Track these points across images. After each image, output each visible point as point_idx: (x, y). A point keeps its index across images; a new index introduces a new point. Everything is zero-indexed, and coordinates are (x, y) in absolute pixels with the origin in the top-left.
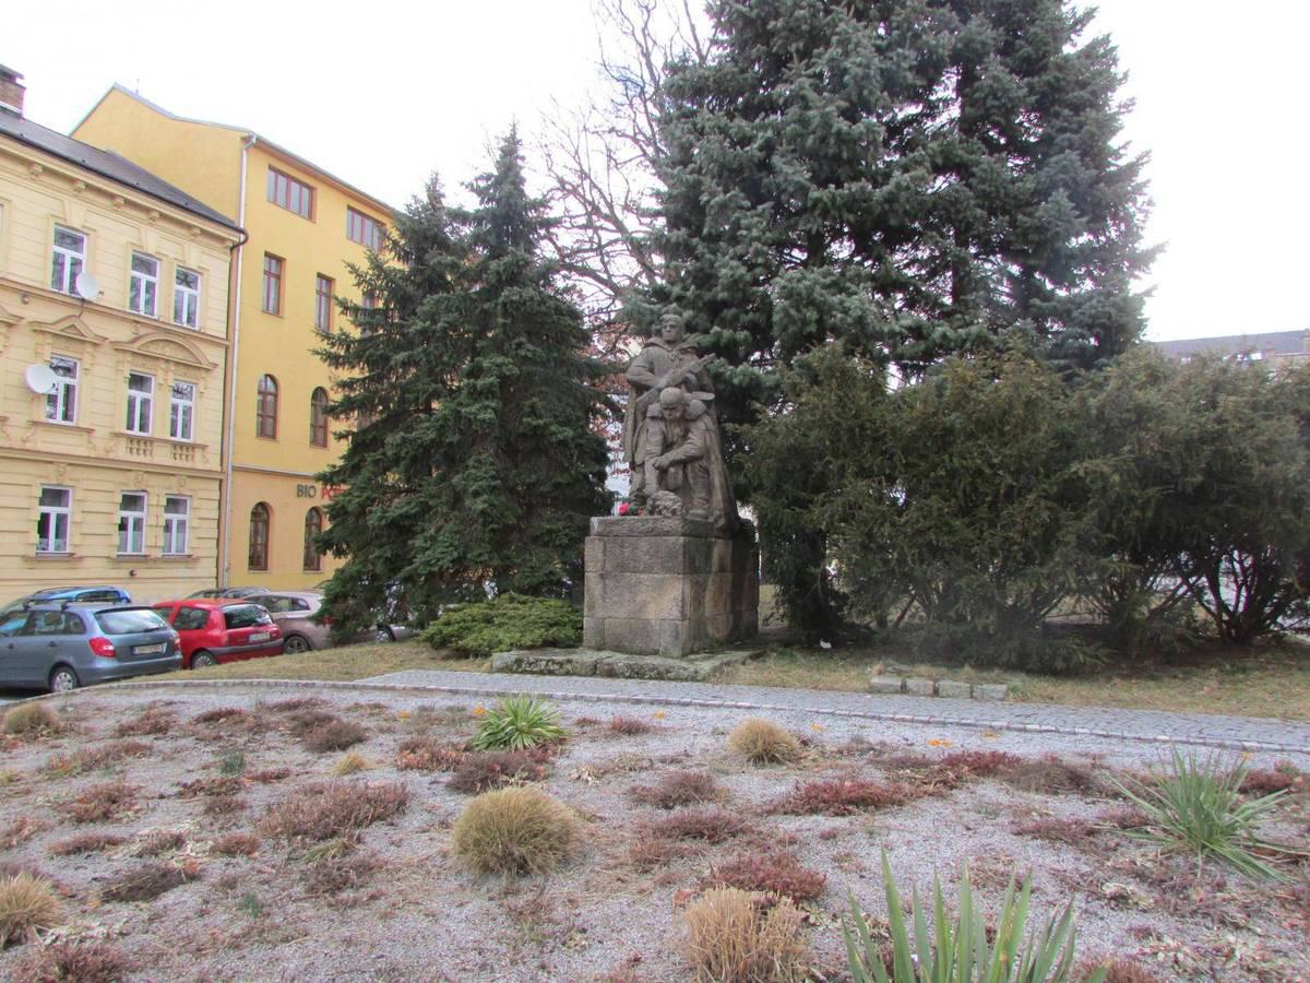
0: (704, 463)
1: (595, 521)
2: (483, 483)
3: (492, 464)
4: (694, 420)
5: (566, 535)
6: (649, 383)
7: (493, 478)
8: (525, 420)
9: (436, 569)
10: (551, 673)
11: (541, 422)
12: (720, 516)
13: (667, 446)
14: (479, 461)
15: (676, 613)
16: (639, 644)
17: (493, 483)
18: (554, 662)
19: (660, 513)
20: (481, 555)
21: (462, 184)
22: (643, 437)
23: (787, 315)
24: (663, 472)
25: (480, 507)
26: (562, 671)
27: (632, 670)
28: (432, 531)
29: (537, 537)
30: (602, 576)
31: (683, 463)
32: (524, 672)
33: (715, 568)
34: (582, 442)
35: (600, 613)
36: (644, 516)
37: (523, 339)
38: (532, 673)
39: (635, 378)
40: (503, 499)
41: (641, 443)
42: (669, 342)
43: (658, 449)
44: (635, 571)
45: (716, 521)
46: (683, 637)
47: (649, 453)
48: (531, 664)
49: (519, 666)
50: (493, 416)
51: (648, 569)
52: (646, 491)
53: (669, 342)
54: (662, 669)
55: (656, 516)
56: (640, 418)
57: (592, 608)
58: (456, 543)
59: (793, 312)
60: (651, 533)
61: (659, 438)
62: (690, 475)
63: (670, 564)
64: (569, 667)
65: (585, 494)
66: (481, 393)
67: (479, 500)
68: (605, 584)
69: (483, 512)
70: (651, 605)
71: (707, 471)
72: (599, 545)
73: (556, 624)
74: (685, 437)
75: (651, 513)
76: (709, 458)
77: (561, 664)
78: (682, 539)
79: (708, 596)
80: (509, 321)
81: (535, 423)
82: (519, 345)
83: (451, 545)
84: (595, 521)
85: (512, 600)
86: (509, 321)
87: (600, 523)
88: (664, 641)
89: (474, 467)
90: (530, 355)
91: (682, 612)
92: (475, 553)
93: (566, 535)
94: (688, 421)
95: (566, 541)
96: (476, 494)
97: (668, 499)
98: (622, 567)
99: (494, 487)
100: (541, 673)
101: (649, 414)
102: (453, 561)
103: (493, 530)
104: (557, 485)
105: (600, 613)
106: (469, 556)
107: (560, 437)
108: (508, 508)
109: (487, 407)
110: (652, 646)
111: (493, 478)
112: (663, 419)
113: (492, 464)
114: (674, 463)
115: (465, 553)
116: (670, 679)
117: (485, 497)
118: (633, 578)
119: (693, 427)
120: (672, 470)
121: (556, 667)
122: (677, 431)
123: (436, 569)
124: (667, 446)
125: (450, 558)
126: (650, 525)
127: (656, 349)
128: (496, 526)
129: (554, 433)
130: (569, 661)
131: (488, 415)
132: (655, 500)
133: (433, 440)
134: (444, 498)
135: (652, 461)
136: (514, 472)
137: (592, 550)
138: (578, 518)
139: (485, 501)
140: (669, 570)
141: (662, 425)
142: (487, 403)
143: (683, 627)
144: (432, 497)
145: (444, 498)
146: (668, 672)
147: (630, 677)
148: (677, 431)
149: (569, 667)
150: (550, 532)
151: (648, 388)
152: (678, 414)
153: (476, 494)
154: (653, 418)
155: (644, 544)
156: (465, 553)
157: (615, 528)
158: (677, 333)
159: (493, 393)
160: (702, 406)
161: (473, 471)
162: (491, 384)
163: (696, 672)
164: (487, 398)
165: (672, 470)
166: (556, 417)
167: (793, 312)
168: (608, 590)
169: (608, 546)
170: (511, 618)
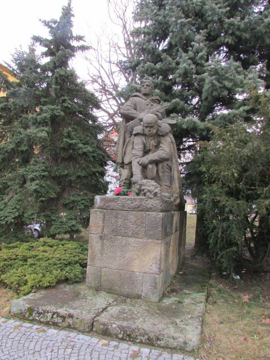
0: (169, 163)
1: (98, 198)
2: (37, 174)
3: (43, 163)
4: (163, 136)
5: (82, 204)
6: (134, 115)
7: (44, 171)
8: (64, 139)
9: (4, 223)
10: (55, 325)
11: (74, 141)
12: (177, 197)
13: (146, 152)
14: (36, 162)
15: (155, 269)
16: (126, 290)
17: (43, 174)
18: (58, 315)
19: (145, 194)
20: (32, 214)
21: (40, 20)
22: (129, 147)
23: (213, 85)
24: (144, 167)
25: (34, 188)
26: (65, 324)
27: (125, 332)
28: (6, 200)
29: (66, 204)
30: (101, 237)
31: (156, 163)
32: (33, 321)
33: (174, 231)
34: (95, 155)
35: (98, 264)
36: (132, 196)
37: (66, 98)
38: (40, 323)
39: (126, 112)
40: (48, 183)
41: (128, 151)
42: (145, 95)
43: (141, 153)
44: (125, 235)
45: (175, 200)
46: (159, 286)
47: (134, 155)
48: (40, 314)
49: (31, 314)
50: (46, 135)
51: (135, 235)
52: (133, 179)
53: (145, 95)
54: (152, 335)
55: (141, 197)
56: (128, 135)
57: (93, 259)
58: (18, 207)
59: (216, 83)
60: (138, 208)
61: (141, 146)
62: (160, 170)
63: (151, 232)
64: (70, 321)
65: (93, 182)
66: (40, 123)
67: (34, 183)
68: (103, 243)
69: (36, 191)
70: (137, 262)
71: (170, 169)
72: (100, 215)
73: (70, 263)
74: (157, 147)
75: (138, 194)
76: (172, 161)
77: (64, 318)
78: (161, 214)
79: (171, 248)
80: (59, 87)
81: (70, 142)
82: (64, 101)
83: (15, 208)
84: (98, 198)
85: (45, 244)
86: (59, 87)
87: (102, 200)
88: (145, 289)
89: (33, 165)
90: (70, 106)
91: (160, 268)
92: (29, 213)
93: (82, 204)
94: (160, 136)
95: (82, 207)
96: (33, 180)
97: (150, 185)
98: (116, 232)
99: (44, 176)
100: (47, 324)
101: (134, 132)
102: (15, 218)
103: (42, 201)
104: (79, 177)
105: (98, 264)
106: (25, 215)
107: (85, 150)
108: (51, 188)
109: (43, 130)
110: (136, 291)
111: (44, 171)
112: (144, 135)
113: (43, 163)
114: (152, 162)
115: (23, 213)
116: (159, 346)
117: (37, 181)
118: (124, 240)
119: (163, 140)
120: (150, 166)
121: (60, 320)
122: (153, 143)
123: (4, 223)
124: (146, 152)
125: (13, 216)
126: (137, 203)
127: (138, 98)
128: (44, 199)
129: (81, 148)
130: (71, 316)
131: (44, 134)
132: (141, 185)
133: (13, 149)
134: (17, 181)
135: (137, 160)
136: (55, 168)
137: (95, 217)
138: (90, 195)
139: (37, 184)
140: (150, 237)
141: (143, 138)
142: (42, 128)
143: (160, 279)
144: (11, 180)
145: (17, 181)
146: (158, 339)
147: (122, 339)
148: (153, 143)
149: (70, 321)
150: (73, 202)
151: (132, 118)
152: (155, 131)
153: (33, 180)
154: (136, 135)
155: (132, 216)
156: (23, 213)
157: (113, 204)
158: (150, 90)
159: (47, 123)
160: (169, 128)
161: (32, 167)
162: (46, 118)
163: (185, 343)
164: (43, 126)
165: (150, 166)
166: (81, 140)
167: (216, 83)
168: (105, 247)
169: (107, 216)
170: (39, 260)
